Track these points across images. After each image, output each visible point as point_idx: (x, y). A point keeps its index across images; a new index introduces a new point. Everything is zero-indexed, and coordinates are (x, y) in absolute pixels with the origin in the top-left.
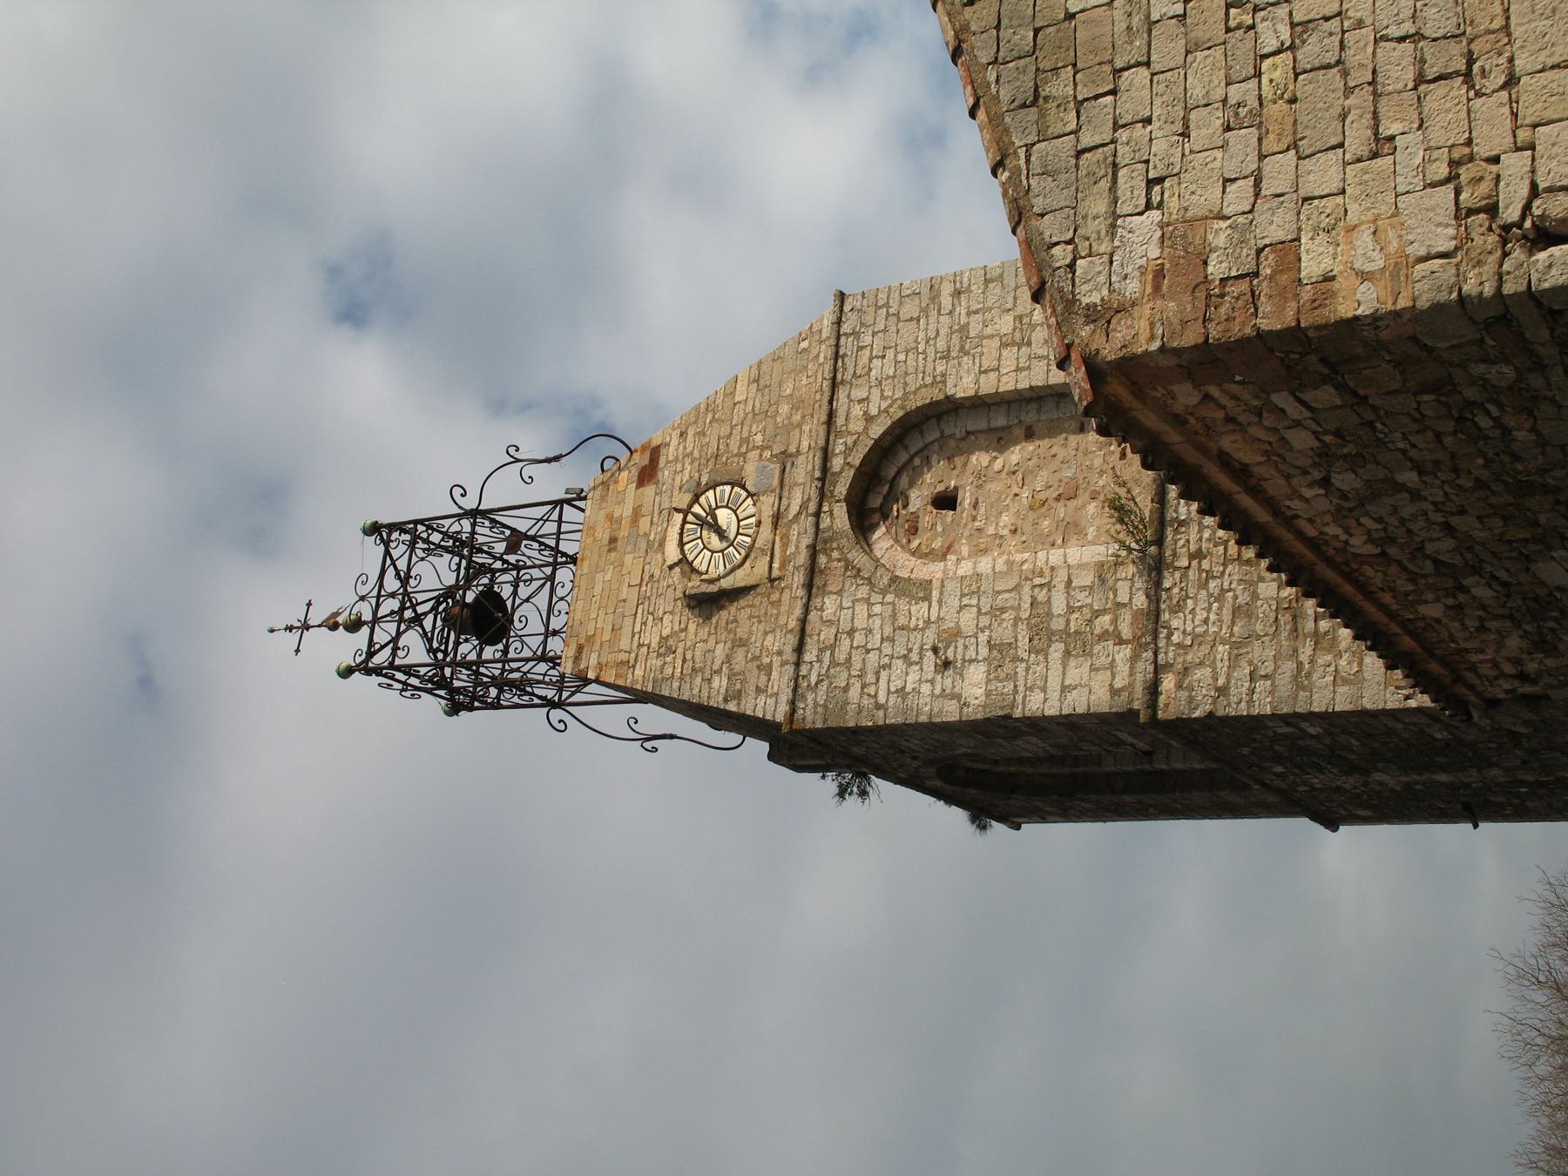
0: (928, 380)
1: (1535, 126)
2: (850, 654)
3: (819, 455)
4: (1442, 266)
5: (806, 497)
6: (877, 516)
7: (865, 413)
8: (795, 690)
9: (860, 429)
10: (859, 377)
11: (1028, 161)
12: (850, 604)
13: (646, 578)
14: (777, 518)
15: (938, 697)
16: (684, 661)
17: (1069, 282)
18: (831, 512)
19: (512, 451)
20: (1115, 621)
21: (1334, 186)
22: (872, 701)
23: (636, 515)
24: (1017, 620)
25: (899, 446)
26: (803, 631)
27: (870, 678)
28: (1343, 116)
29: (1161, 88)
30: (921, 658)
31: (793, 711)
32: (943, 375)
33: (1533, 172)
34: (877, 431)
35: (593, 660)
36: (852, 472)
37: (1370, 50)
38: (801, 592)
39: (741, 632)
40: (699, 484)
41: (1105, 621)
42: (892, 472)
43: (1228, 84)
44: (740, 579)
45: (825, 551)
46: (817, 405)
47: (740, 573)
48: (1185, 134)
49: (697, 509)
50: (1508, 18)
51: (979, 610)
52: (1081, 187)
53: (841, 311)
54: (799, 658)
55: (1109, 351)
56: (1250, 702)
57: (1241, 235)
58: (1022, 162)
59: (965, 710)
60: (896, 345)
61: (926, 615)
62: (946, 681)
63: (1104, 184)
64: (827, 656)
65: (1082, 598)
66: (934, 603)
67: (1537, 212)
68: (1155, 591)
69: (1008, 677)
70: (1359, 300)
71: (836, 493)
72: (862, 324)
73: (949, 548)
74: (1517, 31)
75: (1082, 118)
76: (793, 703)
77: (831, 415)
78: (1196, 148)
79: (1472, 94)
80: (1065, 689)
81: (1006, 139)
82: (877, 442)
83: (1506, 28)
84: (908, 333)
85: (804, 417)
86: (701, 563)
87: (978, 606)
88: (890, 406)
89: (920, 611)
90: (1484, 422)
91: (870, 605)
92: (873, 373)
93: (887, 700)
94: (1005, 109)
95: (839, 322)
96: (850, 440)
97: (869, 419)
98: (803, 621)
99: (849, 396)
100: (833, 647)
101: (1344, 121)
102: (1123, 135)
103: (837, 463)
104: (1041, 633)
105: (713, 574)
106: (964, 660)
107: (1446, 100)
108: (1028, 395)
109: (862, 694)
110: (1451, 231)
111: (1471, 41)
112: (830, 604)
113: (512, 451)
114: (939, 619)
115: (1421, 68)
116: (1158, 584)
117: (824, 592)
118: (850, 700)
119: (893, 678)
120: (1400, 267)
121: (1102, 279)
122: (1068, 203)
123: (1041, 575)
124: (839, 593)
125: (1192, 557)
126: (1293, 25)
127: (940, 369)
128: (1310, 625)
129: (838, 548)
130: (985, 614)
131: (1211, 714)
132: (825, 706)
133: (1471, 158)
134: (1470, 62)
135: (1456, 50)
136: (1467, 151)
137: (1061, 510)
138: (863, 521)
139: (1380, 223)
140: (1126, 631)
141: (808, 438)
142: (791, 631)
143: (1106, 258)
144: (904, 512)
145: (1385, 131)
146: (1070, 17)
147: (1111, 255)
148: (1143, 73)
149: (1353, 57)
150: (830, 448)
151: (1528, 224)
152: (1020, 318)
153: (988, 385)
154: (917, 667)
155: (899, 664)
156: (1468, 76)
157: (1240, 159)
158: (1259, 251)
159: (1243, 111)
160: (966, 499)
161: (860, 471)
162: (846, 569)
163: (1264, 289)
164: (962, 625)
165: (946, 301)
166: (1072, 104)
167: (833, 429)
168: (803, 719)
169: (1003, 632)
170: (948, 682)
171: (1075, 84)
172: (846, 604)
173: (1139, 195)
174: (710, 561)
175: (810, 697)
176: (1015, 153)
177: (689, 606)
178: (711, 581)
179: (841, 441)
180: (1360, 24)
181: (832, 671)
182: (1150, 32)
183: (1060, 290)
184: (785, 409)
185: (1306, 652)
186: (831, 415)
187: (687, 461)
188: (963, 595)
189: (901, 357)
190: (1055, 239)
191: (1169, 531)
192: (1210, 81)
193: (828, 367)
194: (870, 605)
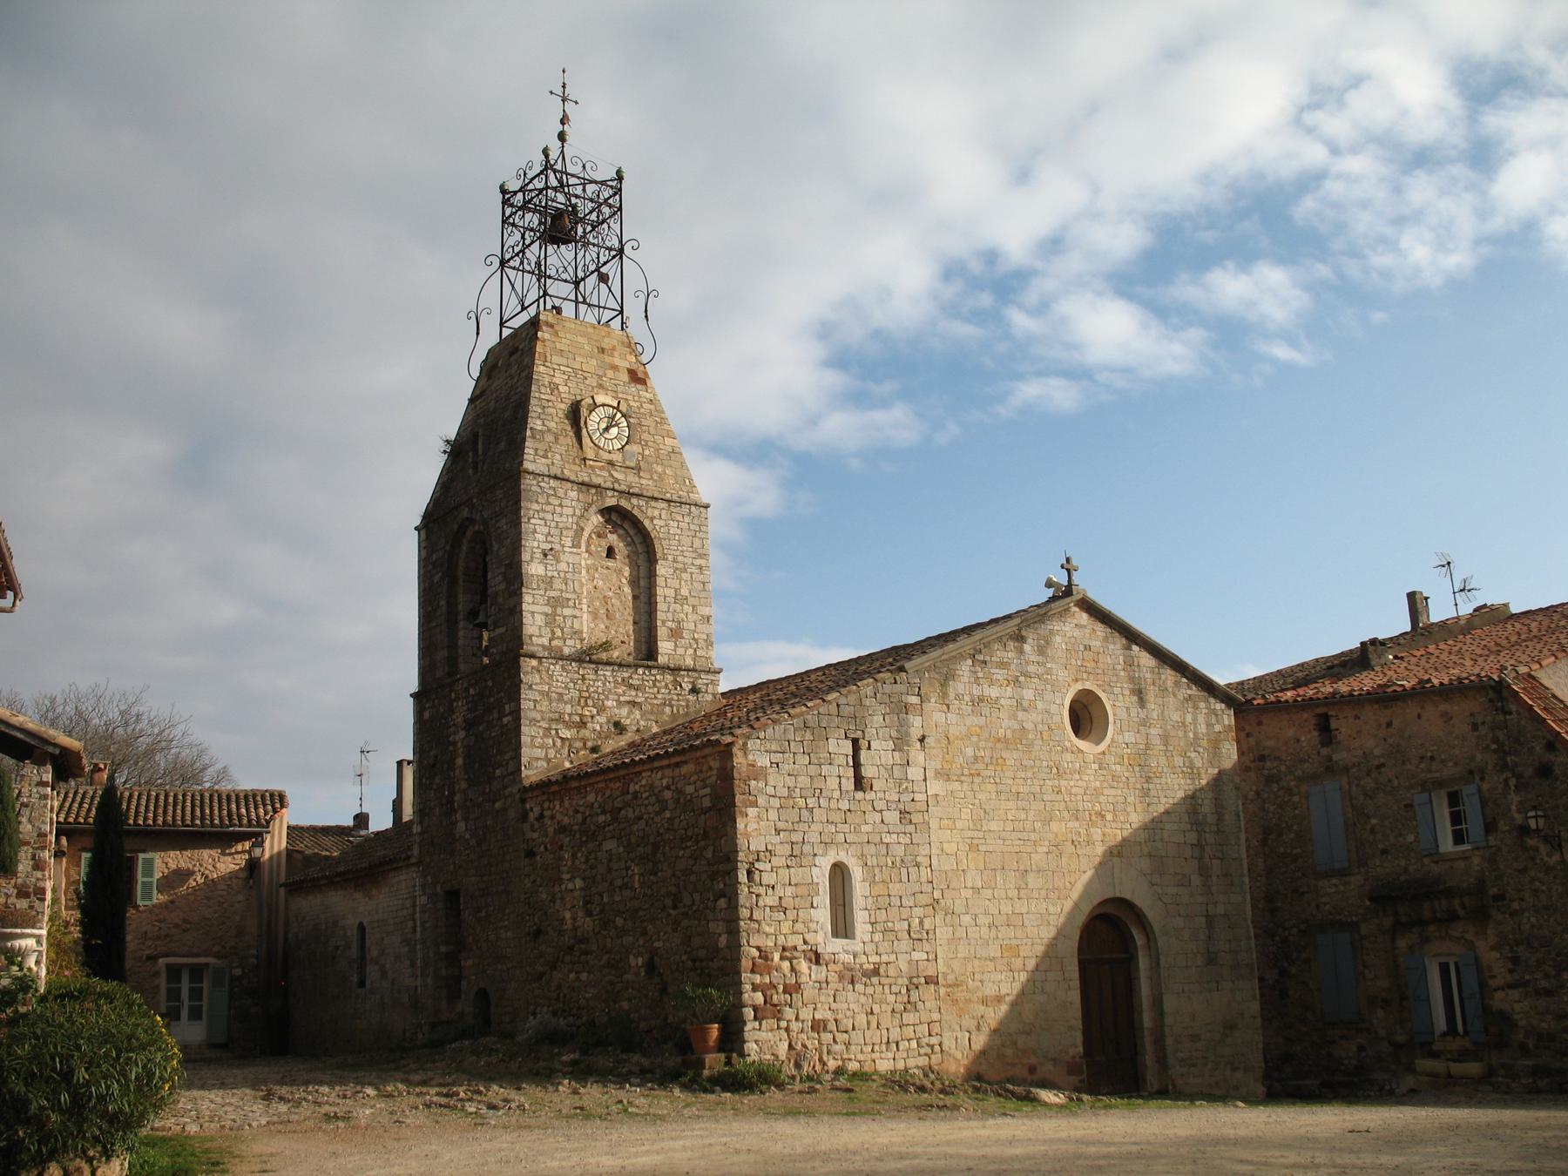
0: (666, 551)
6: (607, 516)
8: (539, 475)
13: (585, 374)
14: (611, 463)
16: (548, 401)
19: (655, 293)
20: (558, 638)
23: (615, 368)
24: (561, 591)
26: (563, 480)
27: (541, 515)
31: (529, 473)
32: (667, 559)
34: (647, 523)
35: (547, 336)
38: (580, 480)
40: (630, 417)
44: (586, 440)
45: (596, 492)
47: (588, 440)
49: (619, 415)
55: (735, 750)
56: (525, 699)
57: (760, 791)
62: (539, 555)
63: (779, 749)
64: (551, 492)
65: (569, 623)
68: (570, 659)
69: (538, 585)
70: (740, 824)
77: (656, 499)
80: (533, 613)
84: (686, 541)
85: (656, 481)
86: (595, 417)
89: (568, 542)
90: (689, 844)
91: (572, 516)
95: (696, 505)
96: (644, 509)
97: (652, 519)
98: (568, 480)
100: (555, 495)
102: (792, 755)
103: (634, 501)
104: (556, 603)
105: (589, 422)
107: (787, 849)
108: (653, 599)
112: (573, 494)
113: (655, 293)
116: (574, 660)
117: (580, 491)
120: (747, 835)
123: (579, 604)
125: (583, 676)
127: (670, 558)
128: (554, 727)
131: (521, 681)
137: (603, 611)
138: (607, 512)
140: (555, 643)
141: (646, 483)
145: (782, 833)
148: (807, 762)
149: (801, 824)
152: (686, 599)
153: (660, 581)
156: (792, 856)
160: (610, 563)
163: (745, 797)
165: (698, 562)
169: (557, 584)
170: (538, 556)
174: (595, 421)
175: (535, 482)
177: (572, 404)
178: (586, 423)
184: (659, 469)
185: (544, 724)
186: (656, 499)
187: (638, 404)
189: (677, 537)
191: (594, 666)
194: (572, 516)
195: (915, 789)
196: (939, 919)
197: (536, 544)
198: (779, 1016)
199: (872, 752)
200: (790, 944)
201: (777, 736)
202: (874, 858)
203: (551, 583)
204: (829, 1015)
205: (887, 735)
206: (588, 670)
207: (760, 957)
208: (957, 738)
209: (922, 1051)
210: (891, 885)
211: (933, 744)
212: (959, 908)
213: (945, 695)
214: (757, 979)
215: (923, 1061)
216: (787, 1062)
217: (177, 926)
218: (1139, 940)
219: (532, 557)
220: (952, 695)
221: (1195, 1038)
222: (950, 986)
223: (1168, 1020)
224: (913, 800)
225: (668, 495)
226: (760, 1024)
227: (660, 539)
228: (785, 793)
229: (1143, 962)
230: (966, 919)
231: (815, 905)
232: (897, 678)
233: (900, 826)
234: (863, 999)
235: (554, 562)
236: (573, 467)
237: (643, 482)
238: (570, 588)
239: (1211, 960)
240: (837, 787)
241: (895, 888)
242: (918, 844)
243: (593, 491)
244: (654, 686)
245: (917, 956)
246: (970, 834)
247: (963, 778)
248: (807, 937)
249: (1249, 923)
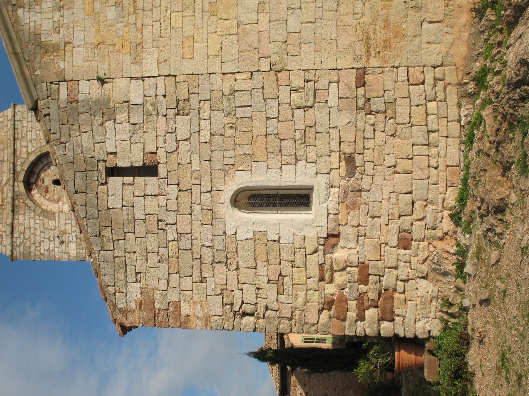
1: (243, 284)
2: (30, 236)
3: (11, 165)
4: (219, 319)
5: (8, 178)
7: (27, 151)
8: (12, 246)
9: (26, 157)
10: (24, 137)
11: (99, 256)
12: (28, 219)
15: (61, 253)
17: (114, 299)
18: (18, 185)
21: (190, 288)
22: (39, 252)
25: (40, 162)
27: (38, 245)
28: (192, 267)
29: (138, 243)
30: (54, 239)
31: (12, 254)
33: (242, 297)
34: (32, 158)
36: (24, 172)
37: (200, 248)
42: (38, 171)
43: (159, 248)
45: (17, 199)
46: (9, 144)
48: (147, 260)
50: (237, 249)
51: (72, 225)
52: (116, 269)
53: (15, 111)
54: (12, 236)
57: (164, 296)
58: (97, 256)
59: (70, 257)
60: (36, 128)
61: (54, 225)
62: (63, 248)
63: (123, 270)
66: (57, 221)
67: (243, 309)
71: (19, 179)
72: (23, 118)
73: (60, 199)
74: (239, 254)
75: (115, 246)
76: (12, 251)
77: (15, 150)
78: (150, 266)
79: (227, 269)
81: (91, 247)
82: (32, 162)
83: (237, 251)
87: (71, 224)
88: (36, 150)
91: (35, 220)
92: (28, 137)
93: (44, 252)
94: (90, 236)
95: (14, 116)
96: (23, 160)
97: (29, 154)
98: (12, 223)
99: (20, 144)
100: (24, 233)
101: (192, 269)
103: (18, 168)
106: (68, 242)
107: (220, 269)
109: (35, 250)
110: (221, 310)
111: (227, 253)
112: (21, 218)
114: (59, 227)
115: (214, 258)
118: (32, 251)
119: (45, 245)
121: (124, 301)
122: (112, 273)
124: (24, 214)
126: (178, 233)
129: (22, 199)
130: (74, 226)
132: (23, 253)
133: (227, 289)
134: (227, 260)
135: (223, 254)
136: (225, 287)
139: (202, 303)
142: (8, 225)
143: (124, 294)
144: (43, 185)
145: (204, 276)
146: (109, 209)
147: (126, 294)
150: (15, 163)
151: (241, 312)
154: (53, 242)
155: (47, 241)
157: (163, 273)
158: (169, 303)
159: (163, 258)
161: (27, 172)
162: (25, 206)
164: (67, 229)
166: (111, 240)
167: (16, 155)
168: (16, 256)
170: (64, 248)
171: (112, 234)
172: (27, 218)
173: (134, 277)
175: (18, 249)
176: (94, 252)
179: (19, 160)
180: (196, 239)
181: (24, 241)
182: (135, 222)
183: (111, 301)
186: (15, 150)
188: (66, 220)
190: (109, 284)
192: (154, 245)
193: (12, 132)
194: (35, 220)
195: (152, 93)
196: (292, 64)
197: (56, 250)
198: (391, 290)
199: (118, 150)
200: (316, 272)
201: (110, 271)
202: (227, 154)
204: (394, 226)
205: (100, 129)
207: (329, 309)
208: (98, 31)
209: (440, 96)
210: (255, 133)
211: (106, 66)
212: (279, 34)
213: (56, 48)
214: (352, 314)
215: (453, 98)
216: (439, 284)
219: (66, 253)
220: (54, 39)
222: (368, 51)
224: (165, 96)
226: (398, 315)
228: (164, 267)
230: (293, 23)
231: (276, 238)
232: (44, 113)
233: (191, 114)
234: (378, 179)
235: (67, 235)
236: (5, 216)
237: (6, 158)
240: (155, 199)
241: (259, 127)
242: (211, 91)
243: (17, 202)
245: (333, 100)
246: (198, 11)
247: (139, 25)
248: (310, 249)
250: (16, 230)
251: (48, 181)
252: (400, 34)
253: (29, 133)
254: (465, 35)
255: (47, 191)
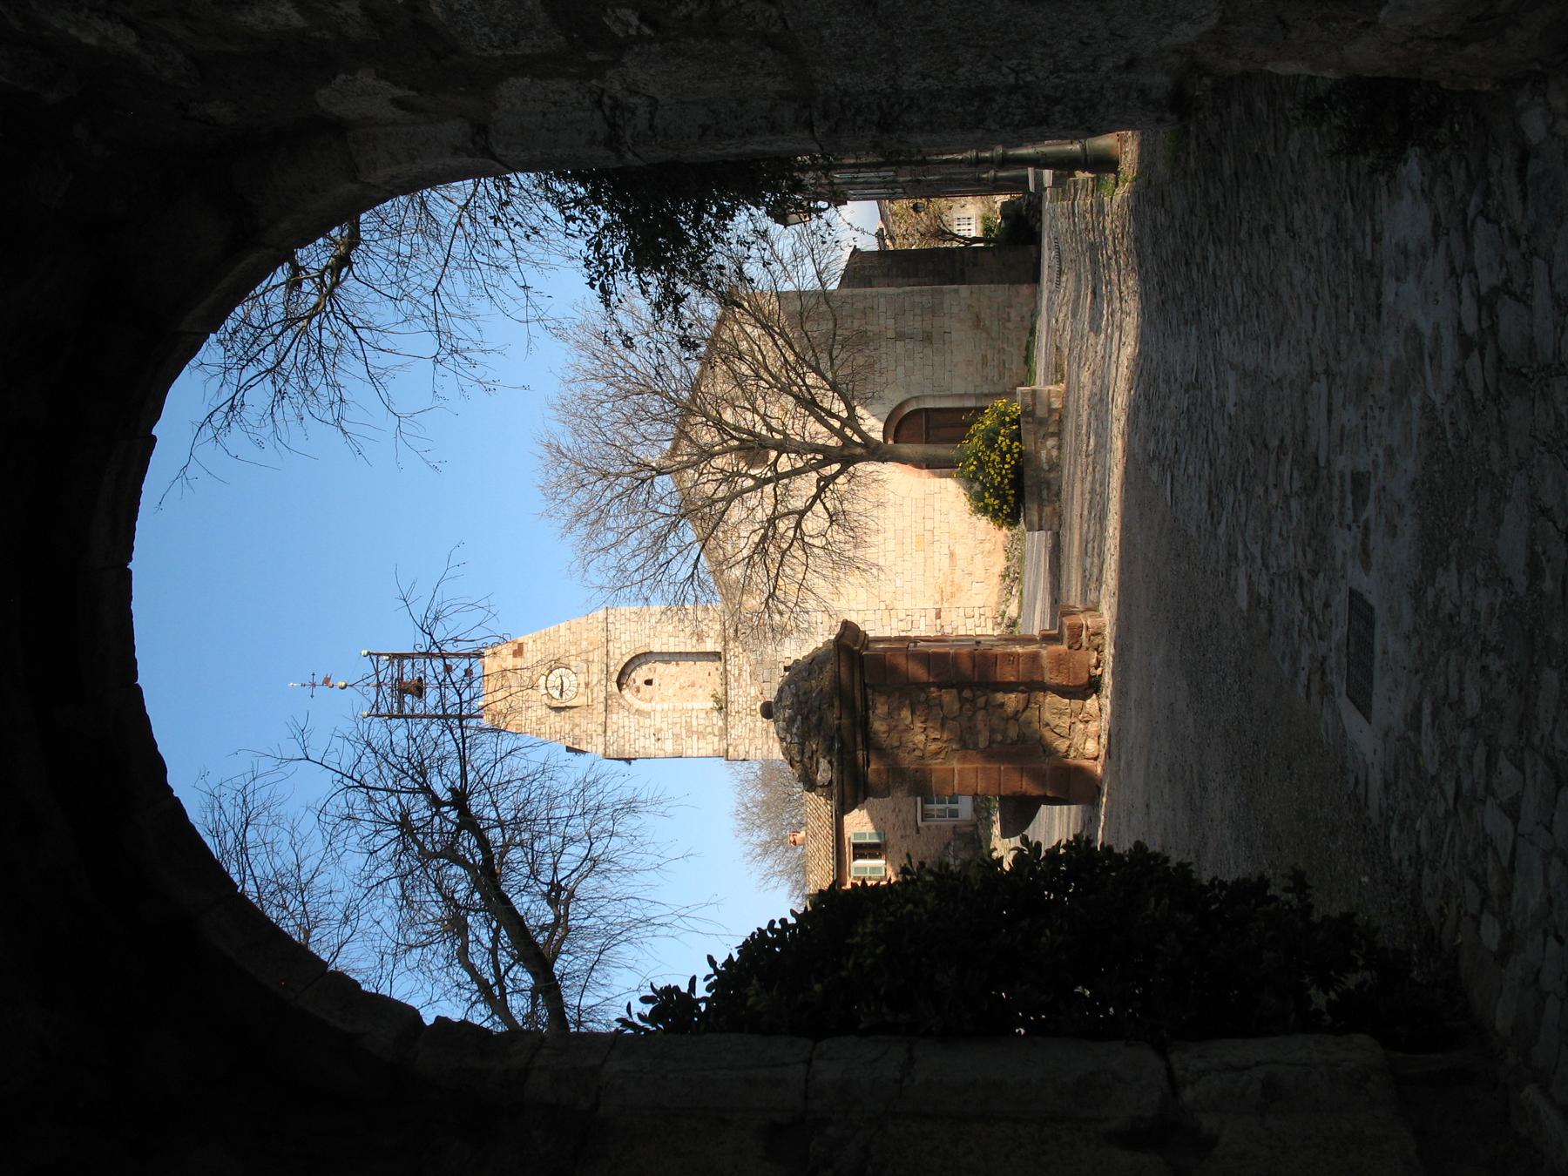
14: (587, 685)
34: (626, 659)
39: (577, 721)
41: (709, 729)
65: (702, 721)
89: (648, 722)
97: (622, 655)
103: (612, 669)
104: (690, 732)
112: (614, 717)
127: (647, 640)
141: (597, 656)
155: (642, 739)
169: (677, 730)
196: (898, 605)
197: (652, 747)
203: (677, 735)
206: (732, 708)
217: (897, 816)
218: (913, 406)
221: (984, 362)
223: (971, 390)
225: (603, 640)
227: (635, 649)
229: (930, 404)
236: (595, 716)
237: (596, 660)
238: (678, 720)
239: (927, 338)
243: (609, 702)
244: (737, 656)
249: (901, 290)
250: (608, 729)
251: (640, 682)
252: (959, 589)
253: (623, 635)
254: (997, 590)
255: (638, 690)
